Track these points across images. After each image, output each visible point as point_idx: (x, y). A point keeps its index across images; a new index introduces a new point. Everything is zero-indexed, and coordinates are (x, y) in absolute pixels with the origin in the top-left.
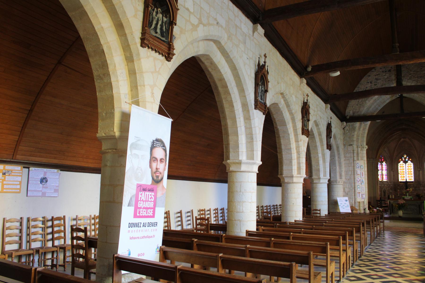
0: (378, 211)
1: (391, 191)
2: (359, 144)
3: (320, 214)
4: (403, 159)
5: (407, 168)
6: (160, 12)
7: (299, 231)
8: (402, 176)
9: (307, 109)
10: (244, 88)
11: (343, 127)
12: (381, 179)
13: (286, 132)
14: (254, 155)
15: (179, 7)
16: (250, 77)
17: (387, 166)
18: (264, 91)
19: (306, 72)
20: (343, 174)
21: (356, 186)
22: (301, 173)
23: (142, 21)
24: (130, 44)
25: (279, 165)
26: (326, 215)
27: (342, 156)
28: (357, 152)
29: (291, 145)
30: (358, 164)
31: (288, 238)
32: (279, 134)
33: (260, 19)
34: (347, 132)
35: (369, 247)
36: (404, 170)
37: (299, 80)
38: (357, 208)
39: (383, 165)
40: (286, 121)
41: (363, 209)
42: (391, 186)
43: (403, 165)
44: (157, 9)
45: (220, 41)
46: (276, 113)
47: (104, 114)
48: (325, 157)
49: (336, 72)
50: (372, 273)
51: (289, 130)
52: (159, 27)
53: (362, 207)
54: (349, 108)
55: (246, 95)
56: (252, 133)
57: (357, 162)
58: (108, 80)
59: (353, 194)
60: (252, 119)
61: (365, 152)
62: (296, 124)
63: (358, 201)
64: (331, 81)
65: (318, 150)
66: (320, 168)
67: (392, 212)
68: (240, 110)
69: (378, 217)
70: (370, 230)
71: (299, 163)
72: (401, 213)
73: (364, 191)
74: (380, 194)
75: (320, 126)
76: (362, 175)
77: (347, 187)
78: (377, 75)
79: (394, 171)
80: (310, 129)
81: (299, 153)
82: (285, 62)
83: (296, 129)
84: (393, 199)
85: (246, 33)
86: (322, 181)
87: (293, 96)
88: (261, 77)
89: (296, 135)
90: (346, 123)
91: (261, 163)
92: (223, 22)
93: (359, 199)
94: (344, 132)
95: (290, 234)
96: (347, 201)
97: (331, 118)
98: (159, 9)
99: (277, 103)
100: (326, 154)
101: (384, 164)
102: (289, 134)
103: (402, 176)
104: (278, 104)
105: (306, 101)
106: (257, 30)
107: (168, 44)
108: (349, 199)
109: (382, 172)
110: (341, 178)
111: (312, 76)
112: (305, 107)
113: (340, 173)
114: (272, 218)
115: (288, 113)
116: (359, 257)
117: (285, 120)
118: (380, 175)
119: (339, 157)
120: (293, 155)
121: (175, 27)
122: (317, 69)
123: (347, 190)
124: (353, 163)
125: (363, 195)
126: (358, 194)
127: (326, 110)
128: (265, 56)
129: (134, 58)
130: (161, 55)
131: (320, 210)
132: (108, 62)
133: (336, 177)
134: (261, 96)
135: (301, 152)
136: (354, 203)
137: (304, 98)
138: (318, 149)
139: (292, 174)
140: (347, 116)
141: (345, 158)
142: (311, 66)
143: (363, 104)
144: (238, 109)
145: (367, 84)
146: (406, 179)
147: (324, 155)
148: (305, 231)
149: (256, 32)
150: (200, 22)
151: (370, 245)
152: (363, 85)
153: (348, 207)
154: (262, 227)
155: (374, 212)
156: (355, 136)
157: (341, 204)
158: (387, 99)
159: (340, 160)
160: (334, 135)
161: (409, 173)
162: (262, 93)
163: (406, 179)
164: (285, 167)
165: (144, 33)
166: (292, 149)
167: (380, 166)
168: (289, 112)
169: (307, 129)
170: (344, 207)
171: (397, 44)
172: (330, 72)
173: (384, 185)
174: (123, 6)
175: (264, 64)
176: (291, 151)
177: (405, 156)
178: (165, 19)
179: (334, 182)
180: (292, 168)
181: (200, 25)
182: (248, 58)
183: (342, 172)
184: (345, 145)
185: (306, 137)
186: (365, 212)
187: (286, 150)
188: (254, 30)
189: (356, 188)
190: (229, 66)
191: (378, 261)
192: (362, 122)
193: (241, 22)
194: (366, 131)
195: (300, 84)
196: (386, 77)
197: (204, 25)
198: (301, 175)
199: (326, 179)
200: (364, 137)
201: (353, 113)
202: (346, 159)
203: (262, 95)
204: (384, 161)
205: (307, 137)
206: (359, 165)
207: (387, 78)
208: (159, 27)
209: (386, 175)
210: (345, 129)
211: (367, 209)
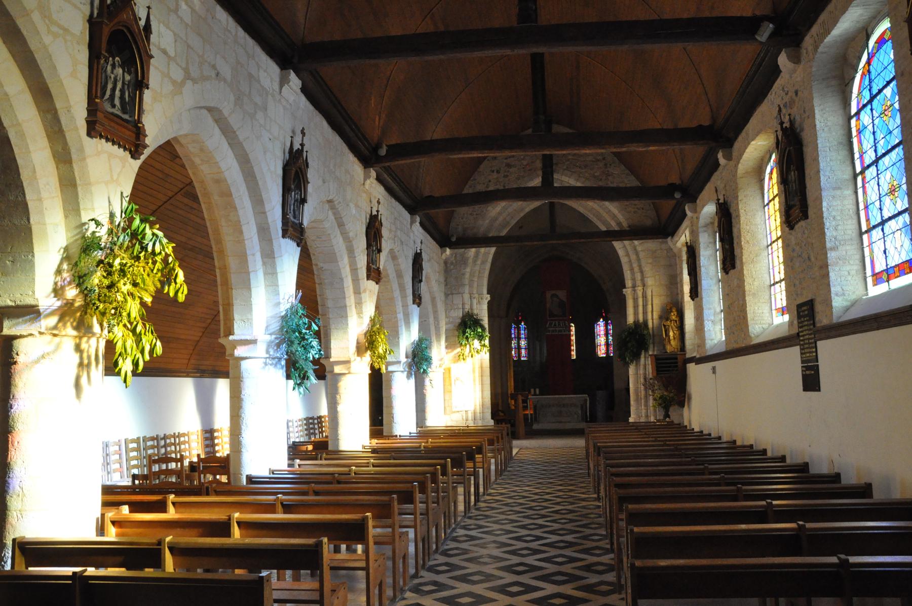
2: (475, 292)
6: (119, 64)
9: (377, 229)
10: (264, 196)
15: (154, 51)
24: (65, 130)
29: (347, 299)
34: (452, 267)
37: (363, 172)
44: (114, 59)
45: (221, 109)
47: (7, 262)
51: (342, 270)
52: (118, 93)
55: (267, 210)
58: (17, 197)
60: (277, 257)
62: (357, 259)
68: (256, 239)
80: (381, 267)
88: (295, 175)
89: (356, 280)
92: (226, 71)
98: (117, 59)
100: (412, 314)
107: (134, 127)
112: (374, 226)
118: (515, 348)
121: (146, 91)
122: (397, 151)
128: (303, 133)
129: (72, 157)
130: (122, 150)
132: (20, 162)
134: (294, 210)
137: (372, 208)
141: (447, 320)
142: (386, 146)
144: (251, 238)
150: (188, 76)
156: (467, 276)
165: (92, 109)
166: (348, 308)
174: (50, 56)
175: (300, 148)
178: (128, 77)
181: (188, 81)
185: (374, 283)
188: (284, 81)
190: (236, 155)
193: (259, 67)
194: (488, 266)
197: (195, 81)
203: (296, 208)
205: (377, 283)
208: (118, 93)
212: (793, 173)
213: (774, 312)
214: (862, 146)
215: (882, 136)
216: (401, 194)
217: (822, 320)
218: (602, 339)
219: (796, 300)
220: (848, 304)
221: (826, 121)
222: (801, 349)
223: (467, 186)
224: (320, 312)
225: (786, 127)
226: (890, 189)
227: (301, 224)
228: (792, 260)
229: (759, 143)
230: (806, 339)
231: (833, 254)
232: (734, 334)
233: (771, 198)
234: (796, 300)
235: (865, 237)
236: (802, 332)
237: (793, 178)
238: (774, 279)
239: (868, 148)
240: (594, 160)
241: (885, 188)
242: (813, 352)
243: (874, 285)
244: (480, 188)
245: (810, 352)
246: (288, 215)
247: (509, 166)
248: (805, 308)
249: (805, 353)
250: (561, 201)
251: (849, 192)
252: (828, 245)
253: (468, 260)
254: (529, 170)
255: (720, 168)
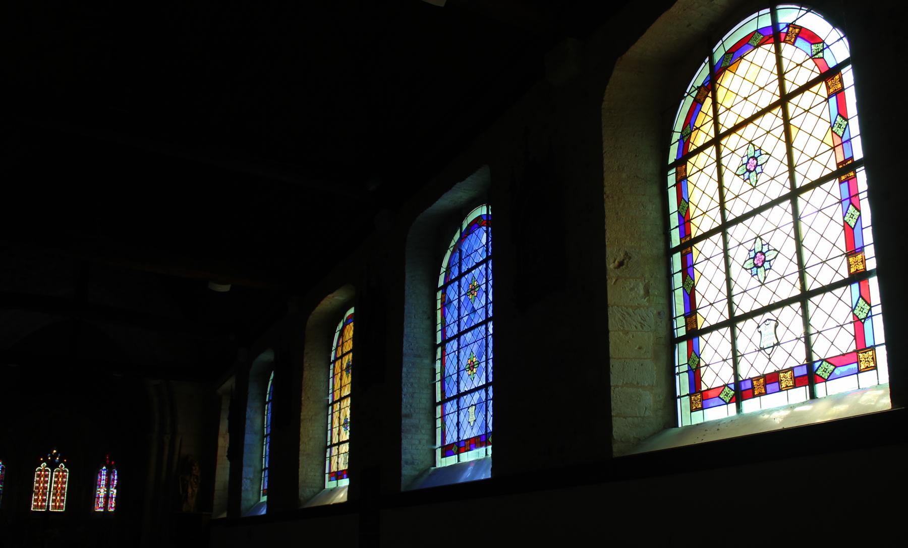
23: (804, 41)
36: (48, 485)
161: (57, 492)
214: (445, 318)
215: (466, 313)
218: (102, 491)
220: (417, 473)
226: (470, 364)
229: (336, 298)
231: (407, 422)
233: (338, 356)
235: (439, 409)
239: (465, 315)
241: (464, 362)
243: (442, 457)
251: (427, 361)
252: (404, 411)
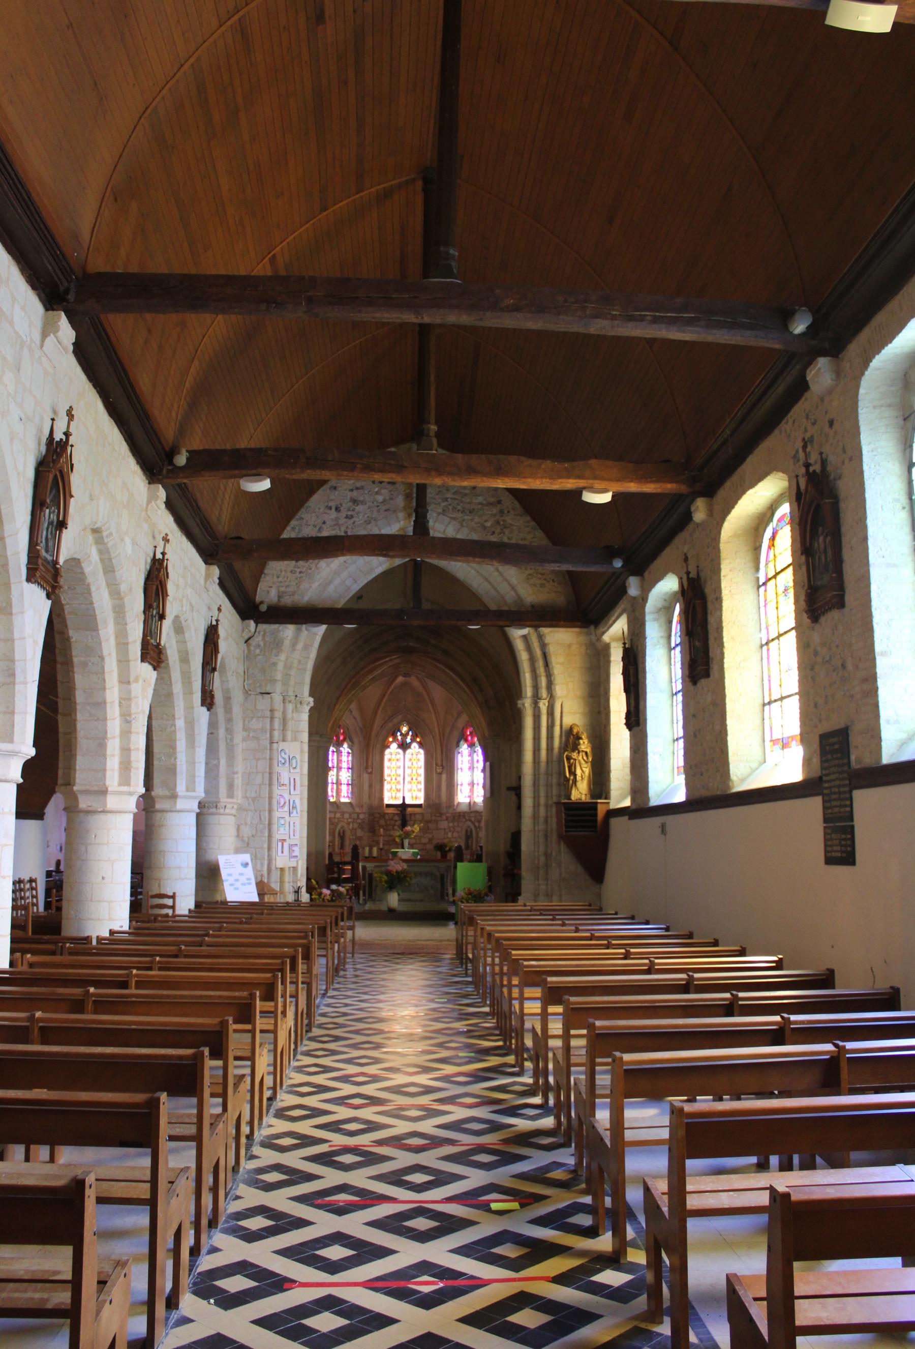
0: (333, 896)
1: (360, 833)
2: (291, 693)
3: (173, 907)
4: (399, 738)
5: (408, 764)
7: (146, 962)
8: (394, 788)
11: (246, 638)
12: (333, 796)
13: (95, 651)
14: (13, 726)
16: (22, 480)
17: (353, 757)
18: (55, 523)
19: (170, 468)
20: (238, 781)
21: (275, 820)
22: (132, 783)
25: (61, 753)
26: (190, 911)
27: (238, 725)
28: (281, 717)
29: (108, 691)
30: (283, 754)
31: (124, 985)
32: (71, 656)
33: (69, 297)
34: (258, 651)
35: (325, 1002)
36: (400, 772)
37: (146, 489)
38: (276, 886)
39: (343, 754)
40: (98, 617)
41: (292, 890)
42: (361, 816)
43: (398, 756)
46: (68, 588)
48: (193, 730)
49: (261, 480)
50: (351, 1069)
51: (103, 644)
53: (289, 882)
54: (267, 578)
56: (14, 656)
57: (282, 745)
59: (266, 845)
61: (305, 717)
62: (128, 627)
63: (280, 865)
64: (230, 497)
65: (176, 708)
66: (178, 763)
67: (370, 896)
69: (342, 914)
70: (325, 953)
71: (126, 751)
72: (393, 899)
73: (297, 836)
74: (330, 842)
75: (187, 635)
76: (295, 785)
77: (249, 822)
78: (357, 488)
79: (371, 773)
81: (128, 718)
82: (116, 431)
83: (127, 644)
84: (374, 858)
85: (24, 338)
86: (180, 804)
87: (128, 541)
89: (123, 662)
90: (257, 623)
91: (32, 752)
93: (282, 860)
94: (249, 650)
95: (129, 975)
96: (246, 865)
97: (219, 610)
99: (79, 560)
101: (345, 749)
102: (102, 658)
103: (394, 788)
104: (81, 561)
105: (161, 557)
106: (56, 330)
108: (252, 860)
109: (338, 775)
110: (231, 795)
111: (185, 481)
112: (157, 576)
113: (228, 778)
114: (32, 924)
115: (107, 590)
116: (307, 1031)
117: (94, 611)
118: (333, 783)
119: (229, 731)
120: (109, 723)
123: (247, 831)
124: (268, 747)
125: (294, 848)
126: (280, 844)
127: (208, 583)
128: (70, 415)
131: (173, 897)
133: (217, 793)
135: (133, 716)
136: (265, 873)
138: (175, 705)
139: (105, 784)
140: (262, 602)
141: (245, 734)
142: (187, 451)
143: (310, 571)
145: (325, 513)
146: (404, 798)
147: (190, 724)
148: (167, 963)
149: (52, 335)
151: (324, 995)
152: (314, 514)
153: (250, 884)
154: (29, 956)
155: (323, 900)
156: (280, 666)
157: (230, 875)
158: (378, 565)
159: (232, 740)
160: (223, 659)
162: (50, 530)
163: (404, 798)
164: (81, 762)
166: (108, 705)
167: (333, 755)
168: (108, 588)
169: (155, 644)
170: (238, 884)
171: (434, 428)
172: (241, 477)
173: (343, 814)
175: (64, 438)
176: (106, 712)
177: (405, 729)
179: (209, 808)
180: (105, 765)
182: (23, 417)
183: (236, 776)
184: (250, 692)
185: (150, 668)
186: (298, 900)
187: (88, 708)
188: (48, 329)
189: (275, 827)
191: (359, 1039)
192: (304, 626)
194: (313, 654)
195: (149, 502)
196: (380, 498)
198: (132, 789)
199: (195, 798)
200: (305, 670)
201: (279, 597)
202: (249, 735)
203: (49, 536)
204: (344, 740)
205: (155, 669)
206: (286, 757)
207: (384, 501)
209: (348, 784)
210: (250, 641)
211: (304, 890)
212: (821, 539)
213: (768, 744)
216: (196, 531)
217: (858, 757)
219: (816, 726)
220: (904, 736)
221: (877, 466)
222: (824, 801)
223: (288, 528)
224: (60, 710)
225: (814, 471)
227: (56, 562)
228: (812, 669)
230: (835, 786)
232: (702, 774)
234: (816, 726)
236: (827, 775)
237: (822, 546)
238: (770, 695)
240: (484, 502)
242: (845, 806)
244: (309, 532)
245: (841, 806)
246: (37, 544)
247: (355, 501)
248: (832, 740)
249: (831, 807)
250: (436, 562)
253: (283, 642)
254: (386, 510)
255: (691, 527)
